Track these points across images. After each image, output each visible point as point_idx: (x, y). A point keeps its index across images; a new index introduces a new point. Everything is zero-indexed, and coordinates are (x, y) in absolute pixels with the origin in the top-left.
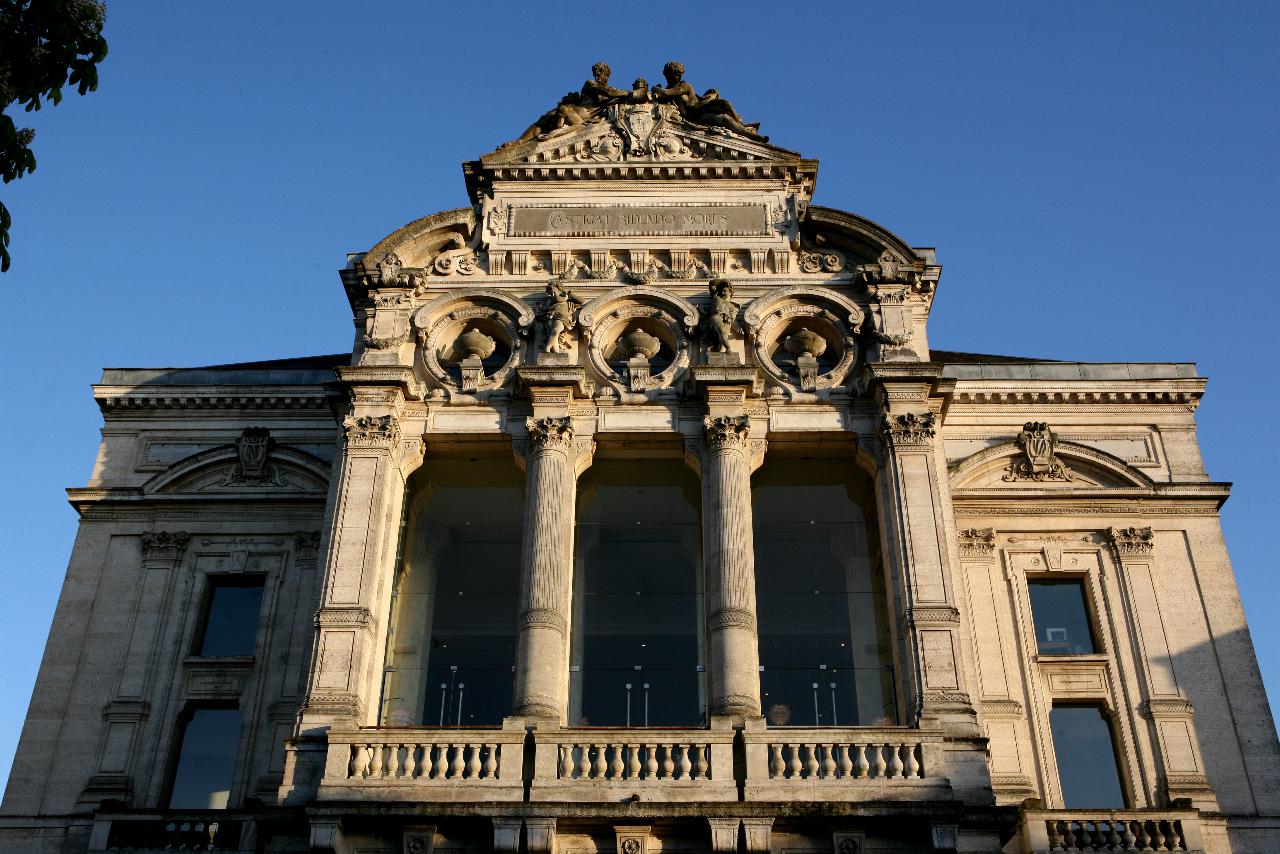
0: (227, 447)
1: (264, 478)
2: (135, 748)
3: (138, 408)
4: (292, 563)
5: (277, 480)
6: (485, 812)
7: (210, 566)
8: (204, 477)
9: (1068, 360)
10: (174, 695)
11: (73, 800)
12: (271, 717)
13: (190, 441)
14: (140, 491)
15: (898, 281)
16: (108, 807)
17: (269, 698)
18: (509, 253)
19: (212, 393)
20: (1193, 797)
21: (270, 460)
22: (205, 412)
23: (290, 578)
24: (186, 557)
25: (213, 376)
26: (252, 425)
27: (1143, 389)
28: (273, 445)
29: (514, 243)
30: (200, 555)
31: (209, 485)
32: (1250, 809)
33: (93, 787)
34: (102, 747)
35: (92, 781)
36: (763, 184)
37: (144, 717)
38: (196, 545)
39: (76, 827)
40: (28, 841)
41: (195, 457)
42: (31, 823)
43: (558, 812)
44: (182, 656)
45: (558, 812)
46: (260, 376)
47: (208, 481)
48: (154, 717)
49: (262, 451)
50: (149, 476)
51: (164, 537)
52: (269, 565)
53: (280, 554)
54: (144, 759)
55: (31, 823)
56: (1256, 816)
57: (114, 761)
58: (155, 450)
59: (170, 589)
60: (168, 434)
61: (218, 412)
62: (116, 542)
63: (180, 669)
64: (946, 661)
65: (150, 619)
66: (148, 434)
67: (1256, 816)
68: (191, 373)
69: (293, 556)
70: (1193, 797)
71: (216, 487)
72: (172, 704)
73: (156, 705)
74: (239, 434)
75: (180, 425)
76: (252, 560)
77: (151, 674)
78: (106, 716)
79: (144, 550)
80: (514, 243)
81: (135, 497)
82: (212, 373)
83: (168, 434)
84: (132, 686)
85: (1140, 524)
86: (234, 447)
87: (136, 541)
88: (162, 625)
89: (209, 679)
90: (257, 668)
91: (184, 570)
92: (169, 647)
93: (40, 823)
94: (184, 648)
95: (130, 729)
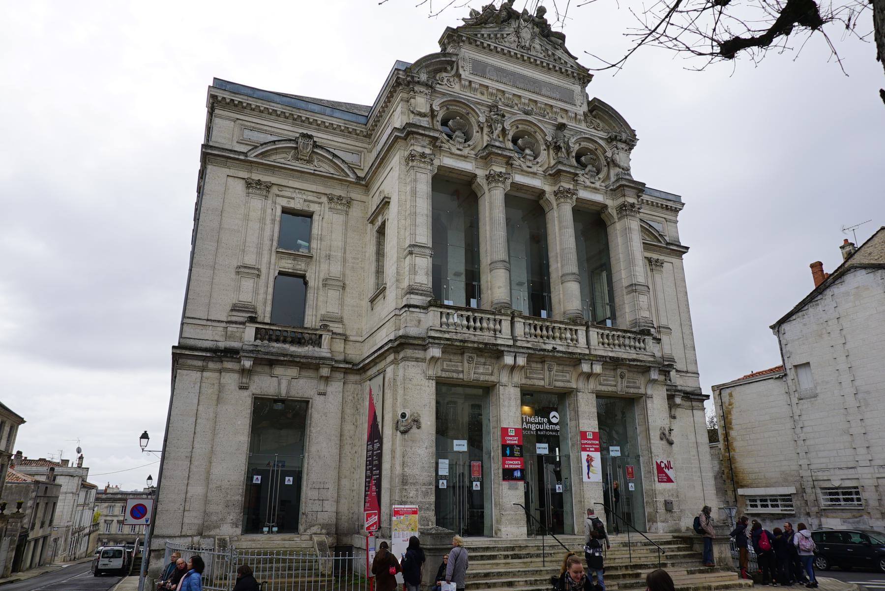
0: (290, 140)
1: (310, 161)
2: (256, 292)
3: (236, 106)
4: (327, 209)
5: (315, 163)
6: (502, 348)
7: (284, 202)
8: (276, 154)
9: (879, 234)
10: (272, 267)
11: (225, 314)
12: (325, 285)
13: (277, 134)
14: (245, 154)
15: (625, 142)
16: (253, 320)
17: (322, 276)
18: (470, 82)
19: (279, 108)
20: (331, 324)
21: (313, 152)
22: (273, 117)
23: (326, 217)
24: (270, 196)
25: (277, 99)
26: (305, 132)
27: (665, 203)
28: (315, 146)
29: (473, 78)
30: (278, 196)
31: (279, 159)
32: (685, 369)
33: (235, 308)
34: (238, 289)
35: (234, 305)
36: (573, 80)
37: (258, 276)
38: (275, 190)
39: (232, 328)
40: (204, 331)
41: (274, 142)
42: (204, 323)
43: (530, 351)
44: (274, 248)
45: (530, 351)
46: (303, 105)
47: (278, 156)
48: (263, 277)
49: (310, 147)
50: (250, 148)
51: (259, 182)
52: (313, 208)
53: (320, 203)
54: (261, 297)
55: (204, 323)
56: (687, 372)
57: (246, 297)
58: (247, 132)
59: (264, 211)
60: (253, 125)
61: (255, 113)
62: (230, 179)
63: (274, 254)
64: (646, 307)
65: (255, 226)
66: (240, 122)
67: (687, 372)
68: (264, 94)
69: (327, 206)
70: (331, 324)
71: (282, 161)
72: (272, 271)
73: (264, 270)
74: (298, 135)
75: (330, 137)
76: (307, 203)
77: (259, 254)
78: (238, 273)
79: (248, 188)
80: (473, 78)
81: (242, 157)
82: (278, 96)
83: (253, 125)
84: (250, 260)
85: (661, 258)
86: (295, 141)
87: (243, 182)
88: (262, 229)
89: (290, 261)
90: (314, 259)
91: (270, 202)
92: (267, 242)
93: (209, 323)
94: (275, 244)
95: (252, 281)
